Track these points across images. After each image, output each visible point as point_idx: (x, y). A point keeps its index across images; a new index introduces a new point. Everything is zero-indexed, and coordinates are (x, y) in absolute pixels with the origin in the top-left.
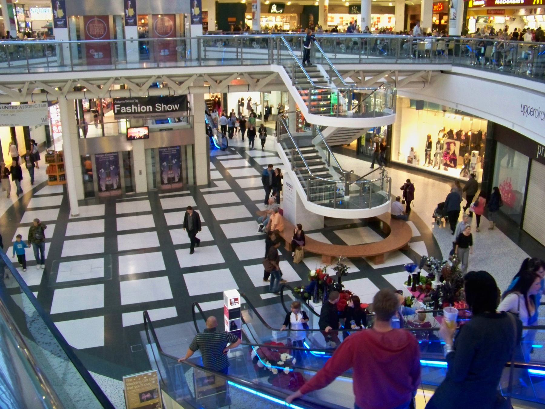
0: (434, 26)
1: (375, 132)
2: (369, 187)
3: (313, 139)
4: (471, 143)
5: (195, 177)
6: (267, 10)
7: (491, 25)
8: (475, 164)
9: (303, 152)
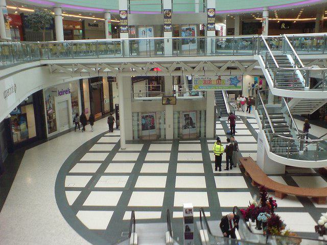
5: (205, 133)
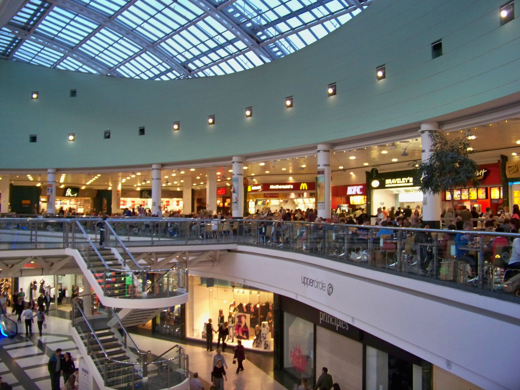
0: (219, 208)
1: (169, 311)
2: (167, 366)
3: (108, 321)
4: (260, 315)
6: (62, 194)
7: (268, 206)
8: (266, 334)
9: (100, 335)
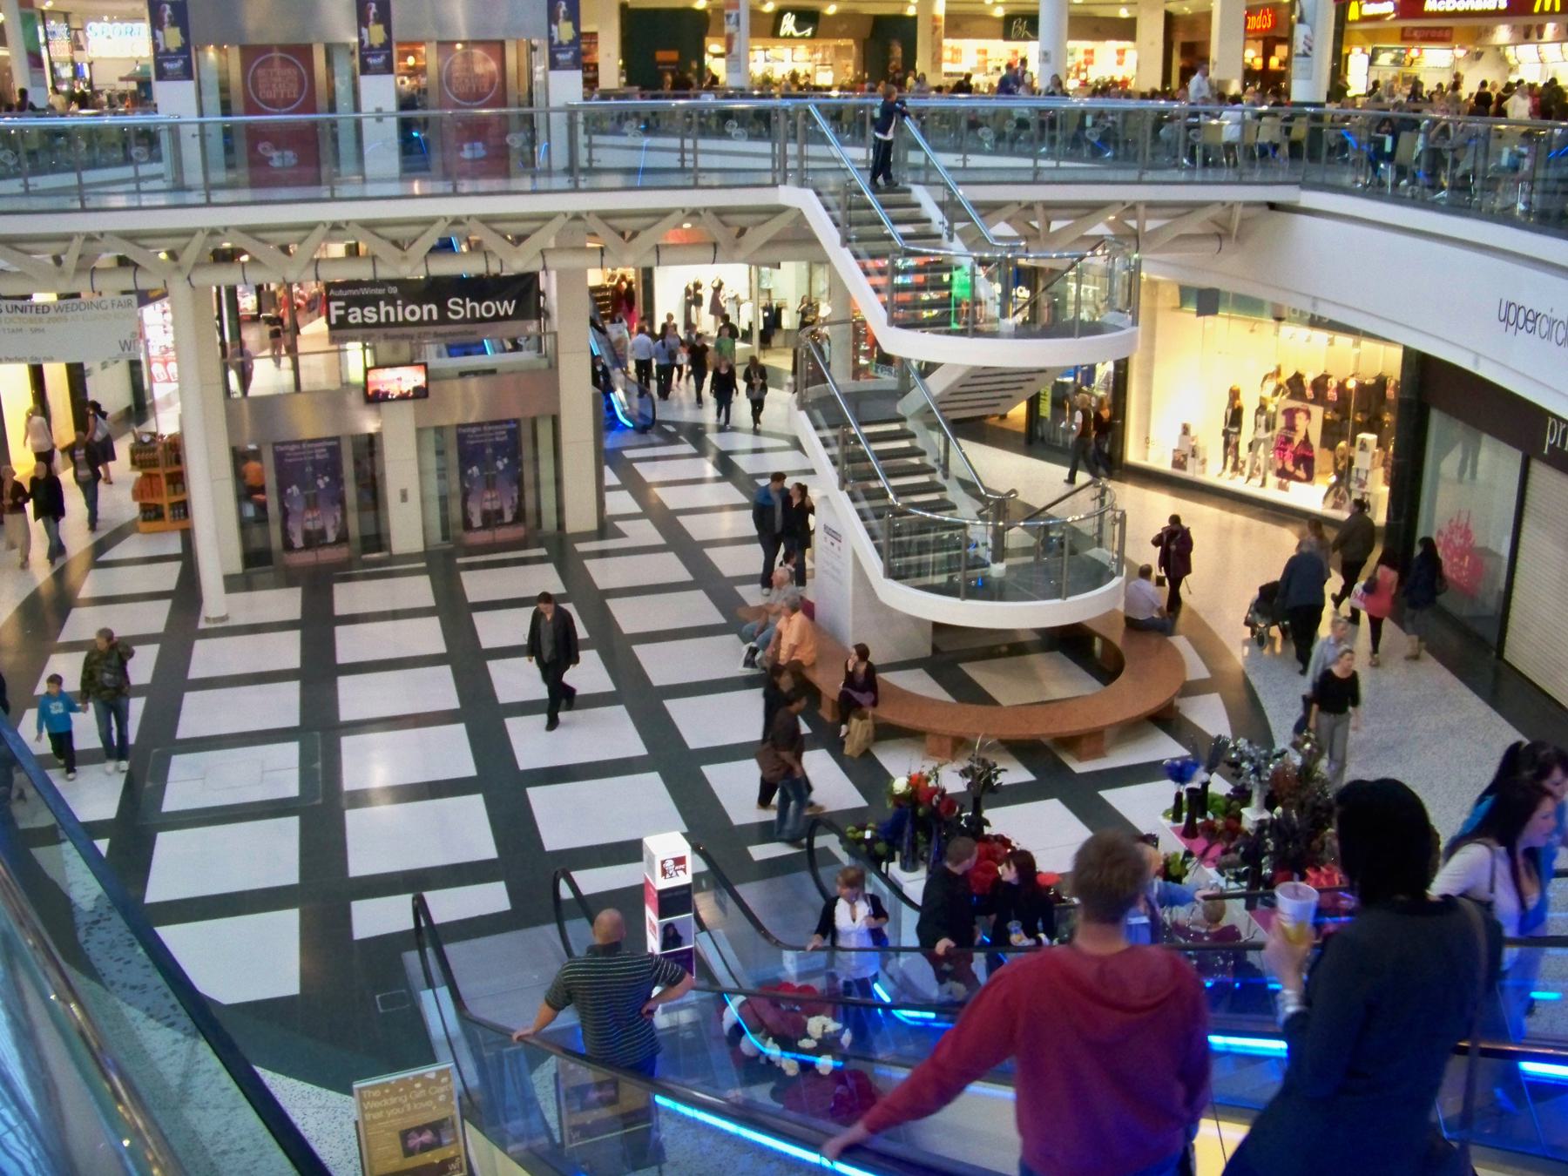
0: (1249, 75)
1: (1079, 381)
2: (1062, 538)
3: (900, 398)
4: (1355, 412)
5: (560, 510)
6: (769, 28)
7: (1414, 71)
8: (1367, 472)
9: (873, 438)
